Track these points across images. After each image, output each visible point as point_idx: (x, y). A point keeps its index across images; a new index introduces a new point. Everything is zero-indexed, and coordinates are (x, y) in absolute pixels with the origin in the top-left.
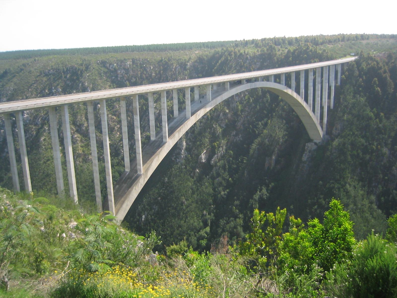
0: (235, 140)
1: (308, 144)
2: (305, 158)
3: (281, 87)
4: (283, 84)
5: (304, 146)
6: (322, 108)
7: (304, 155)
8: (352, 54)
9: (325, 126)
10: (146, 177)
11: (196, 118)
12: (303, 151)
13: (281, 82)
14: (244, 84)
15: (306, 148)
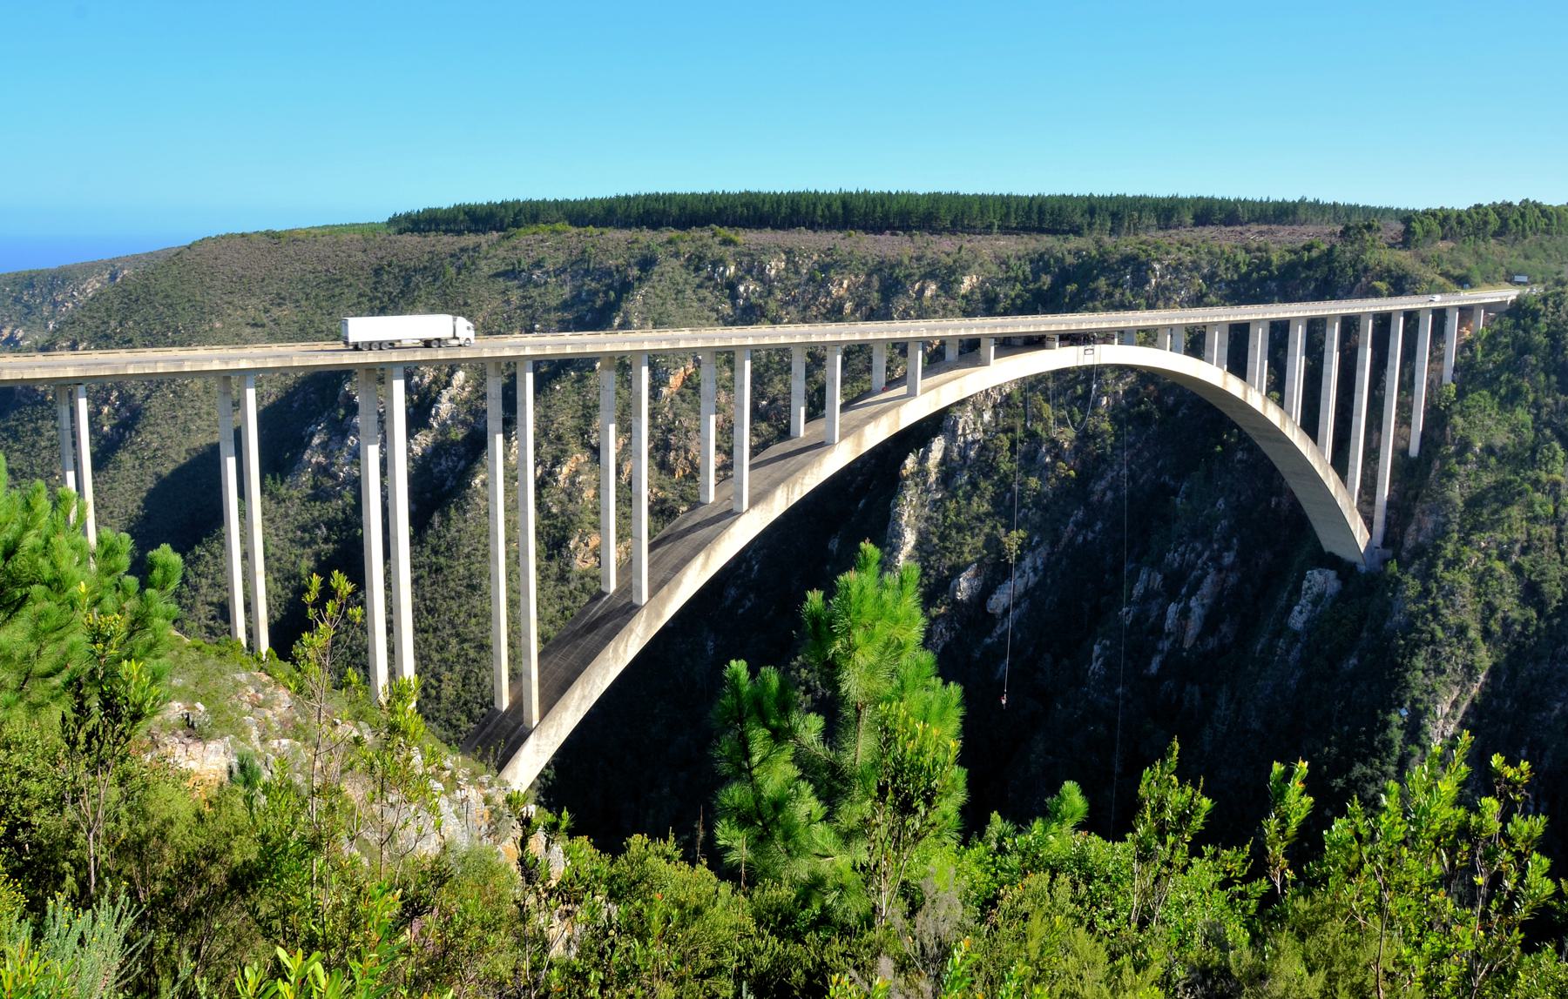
0: (1080, 539)
1: (1315, 572)
2: (1297, 620)
3: (1211, 372)
4: (1211, 361)
5: (1302, 577)
6: (1372, 454)
7: (1297, 608)
8: (1518, 279)
9: (1379, 517)
10: (659, 616)
11: (859, 445)
12: (1297, 591)
13: (1207, 354)
14: (1052, 348)
15: (1306, 584)
